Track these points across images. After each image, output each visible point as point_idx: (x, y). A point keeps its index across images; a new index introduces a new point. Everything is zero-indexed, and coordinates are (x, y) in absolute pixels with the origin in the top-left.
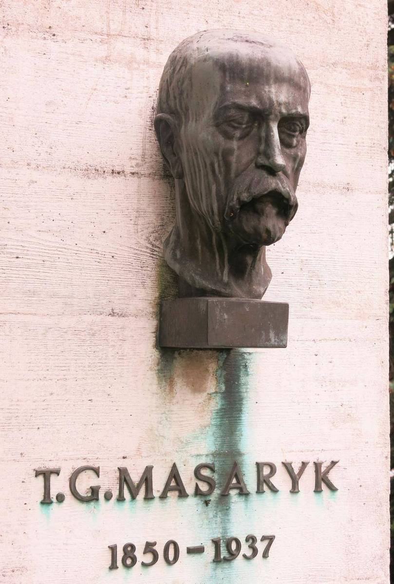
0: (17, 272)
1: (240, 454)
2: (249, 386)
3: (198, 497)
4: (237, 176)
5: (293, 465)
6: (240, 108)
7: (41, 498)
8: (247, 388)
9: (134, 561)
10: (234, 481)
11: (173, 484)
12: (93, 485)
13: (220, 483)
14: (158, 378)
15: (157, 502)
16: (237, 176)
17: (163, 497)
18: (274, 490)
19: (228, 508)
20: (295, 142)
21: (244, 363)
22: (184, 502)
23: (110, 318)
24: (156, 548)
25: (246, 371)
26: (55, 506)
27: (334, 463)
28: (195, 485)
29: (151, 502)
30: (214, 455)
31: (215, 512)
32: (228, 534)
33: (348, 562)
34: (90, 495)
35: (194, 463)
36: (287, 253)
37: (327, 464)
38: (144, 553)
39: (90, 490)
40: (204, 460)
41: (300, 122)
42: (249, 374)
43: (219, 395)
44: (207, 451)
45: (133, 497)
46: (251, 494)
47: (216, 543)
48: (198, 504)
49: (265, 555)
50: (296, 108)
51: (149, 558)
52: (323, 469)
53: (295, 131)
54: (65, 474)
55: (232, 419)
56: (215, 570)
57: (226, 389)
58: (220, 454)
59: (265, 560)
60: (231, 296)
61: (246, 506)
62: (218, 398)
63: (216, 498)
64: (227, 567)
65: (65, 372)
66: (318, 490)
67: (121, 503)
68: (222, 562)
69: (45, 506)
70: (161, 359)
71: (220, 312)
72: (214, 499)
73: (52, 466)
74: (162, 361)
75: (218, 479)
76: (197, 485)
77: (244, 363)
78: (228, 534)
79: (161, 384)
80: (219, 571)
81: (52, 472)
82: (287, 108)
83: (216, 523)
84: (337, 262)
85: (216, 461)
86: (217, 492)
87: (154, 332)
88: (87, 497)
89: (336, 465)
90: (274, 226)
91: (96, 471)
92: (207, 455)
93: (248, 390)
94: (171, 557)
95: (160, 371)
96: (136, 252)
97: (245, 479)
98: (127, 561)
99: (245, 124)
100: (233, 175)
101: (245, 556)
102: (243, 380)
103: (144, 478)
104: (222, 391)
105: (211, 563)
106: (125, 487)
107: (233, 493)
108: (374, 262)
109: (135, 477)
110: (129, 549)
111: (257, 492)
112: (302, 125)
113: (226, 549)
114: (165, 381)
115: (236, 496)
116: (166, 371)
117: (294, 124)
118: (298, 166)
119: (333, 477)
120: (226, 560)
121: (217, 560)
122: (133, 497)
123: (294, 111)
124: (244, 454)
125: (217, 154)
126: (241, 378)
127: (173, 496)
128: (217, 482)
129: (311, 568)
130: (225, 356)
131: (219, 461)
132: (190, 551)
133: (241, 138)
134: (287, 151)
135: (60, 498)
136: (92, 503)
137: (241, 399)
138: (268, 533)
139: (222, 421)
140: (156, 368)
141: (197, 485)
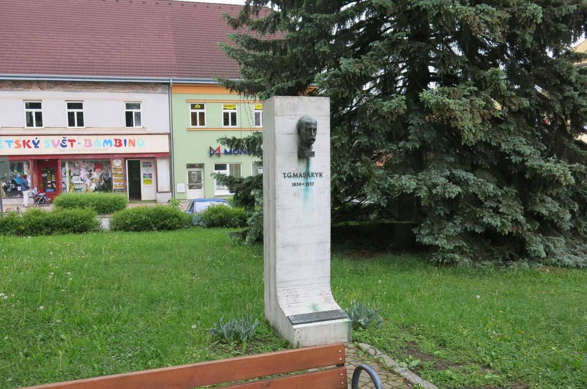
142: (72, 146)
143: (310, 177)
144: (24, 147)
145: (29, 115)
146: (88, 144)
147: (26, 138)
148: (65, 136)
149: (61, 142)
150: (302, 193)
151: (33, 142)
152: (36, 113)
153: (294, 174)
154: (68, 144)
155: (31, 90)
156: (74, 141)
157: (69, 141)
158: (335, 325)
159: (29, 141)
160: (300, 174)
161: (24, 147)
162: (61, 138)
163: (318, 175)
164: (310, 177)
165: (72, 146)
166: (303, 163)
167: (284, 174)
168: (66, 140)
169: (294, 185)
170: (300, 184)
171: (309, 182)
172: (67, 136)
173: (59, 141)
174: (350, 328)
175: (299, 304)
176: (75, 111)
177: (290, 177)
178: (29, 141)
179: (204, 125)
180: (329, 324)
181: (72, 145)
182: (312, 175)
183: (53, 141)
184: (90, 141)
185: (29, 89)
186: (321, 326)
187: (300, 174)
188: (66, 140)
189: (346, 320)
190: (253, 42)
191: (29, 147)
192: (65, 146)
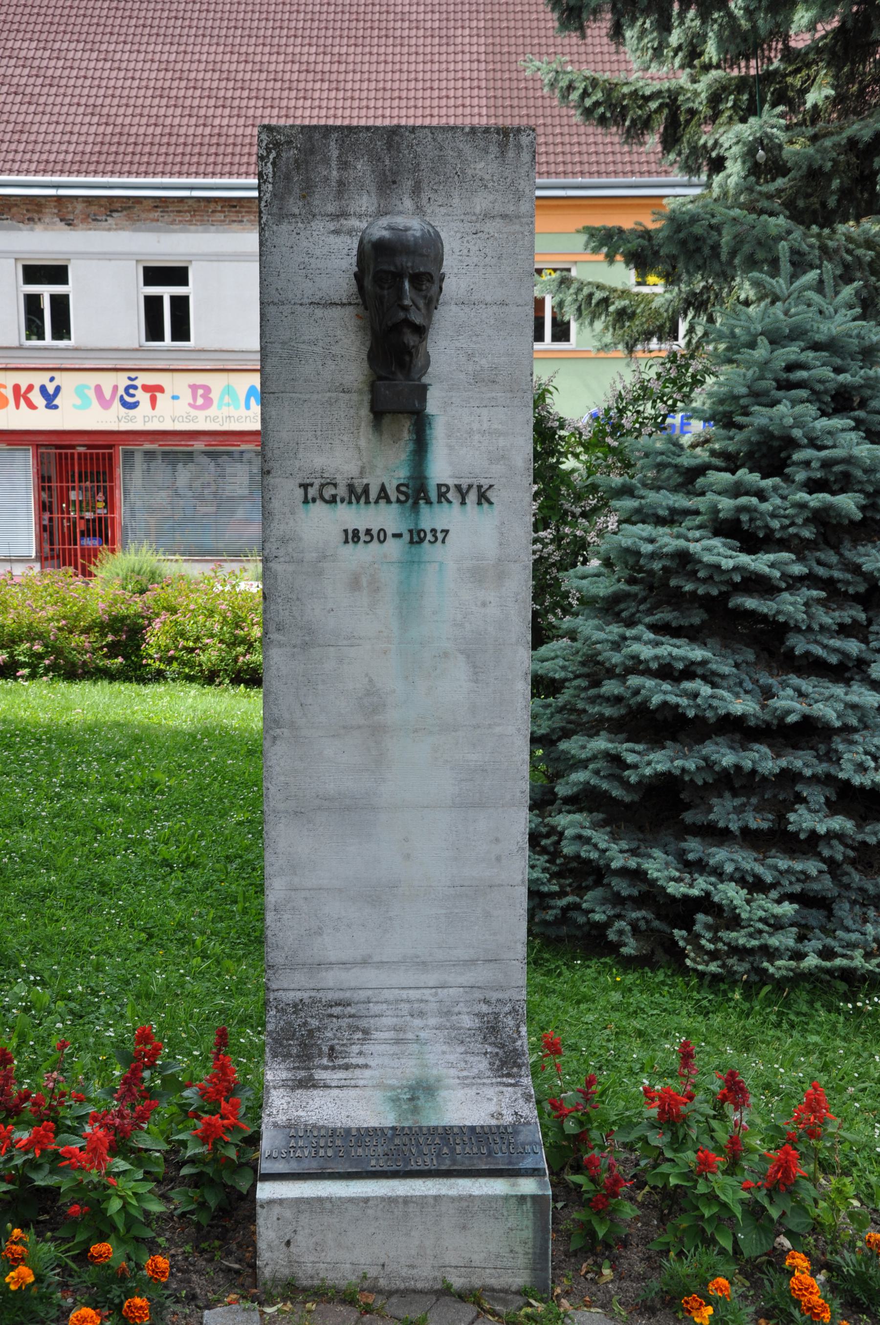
1: (425, 478)
17: (376, 502)
18: (449, 502)
27: (491, 486)
35: (395, 483)
45: (358, 502)
47: (411, 531)
49: (443, 541)
51: (368, 538)
54: (316, 486)
66: (479, 503)
86: (410, 501)
91: (335, 485)
94: (382, 538)
107: (422, 502)
109: (359, 490)
119: (489, 494)
121: (411, 542)
122: (358, 502)
135: (314, 500)
142: (153, 407)
143: (429, 502)
144: (17, 406)
145: (32, 303)
146: (200, 401)
147: (23, 380)
148: (133, 375)
149: (121, 391)
150: (390, 577)
151: (43, 389)
152: (54, 298)
153: (351, 488)
154: (142, 397)
155: (39, 227)
156: (160, 389)
157: (146, 388)
158: (467, 1201)
159: (30, 388)
160: (383, 488)
161: (17, 406)
162: (122, 380)
163: (472, 497)
164: (429, 502)
165: (153, 407)
166: (396, 439)
167: (305, 486)
168: (135, 387)
169: (353, 537)
170: (381, 536)
171: (439, 528)
172: (139, 374)
173: (116, 388)
174: (545, 1230)
175: (358, 1072)
176: (166, 292)
177: (333, 500)
178: (30, 388)
179: (568, 340)
180: (437, 1198)
181: (153, 401)
182: (442, 496)
183: (98, 389)
184: (207, 389)
185: (31, 224)
186: (391, 1201)
187: (383, 488)
188: (135, 387)
189: (528, 1186)
190: (696, 35)
191: (31, 406)
192: (134, 406)
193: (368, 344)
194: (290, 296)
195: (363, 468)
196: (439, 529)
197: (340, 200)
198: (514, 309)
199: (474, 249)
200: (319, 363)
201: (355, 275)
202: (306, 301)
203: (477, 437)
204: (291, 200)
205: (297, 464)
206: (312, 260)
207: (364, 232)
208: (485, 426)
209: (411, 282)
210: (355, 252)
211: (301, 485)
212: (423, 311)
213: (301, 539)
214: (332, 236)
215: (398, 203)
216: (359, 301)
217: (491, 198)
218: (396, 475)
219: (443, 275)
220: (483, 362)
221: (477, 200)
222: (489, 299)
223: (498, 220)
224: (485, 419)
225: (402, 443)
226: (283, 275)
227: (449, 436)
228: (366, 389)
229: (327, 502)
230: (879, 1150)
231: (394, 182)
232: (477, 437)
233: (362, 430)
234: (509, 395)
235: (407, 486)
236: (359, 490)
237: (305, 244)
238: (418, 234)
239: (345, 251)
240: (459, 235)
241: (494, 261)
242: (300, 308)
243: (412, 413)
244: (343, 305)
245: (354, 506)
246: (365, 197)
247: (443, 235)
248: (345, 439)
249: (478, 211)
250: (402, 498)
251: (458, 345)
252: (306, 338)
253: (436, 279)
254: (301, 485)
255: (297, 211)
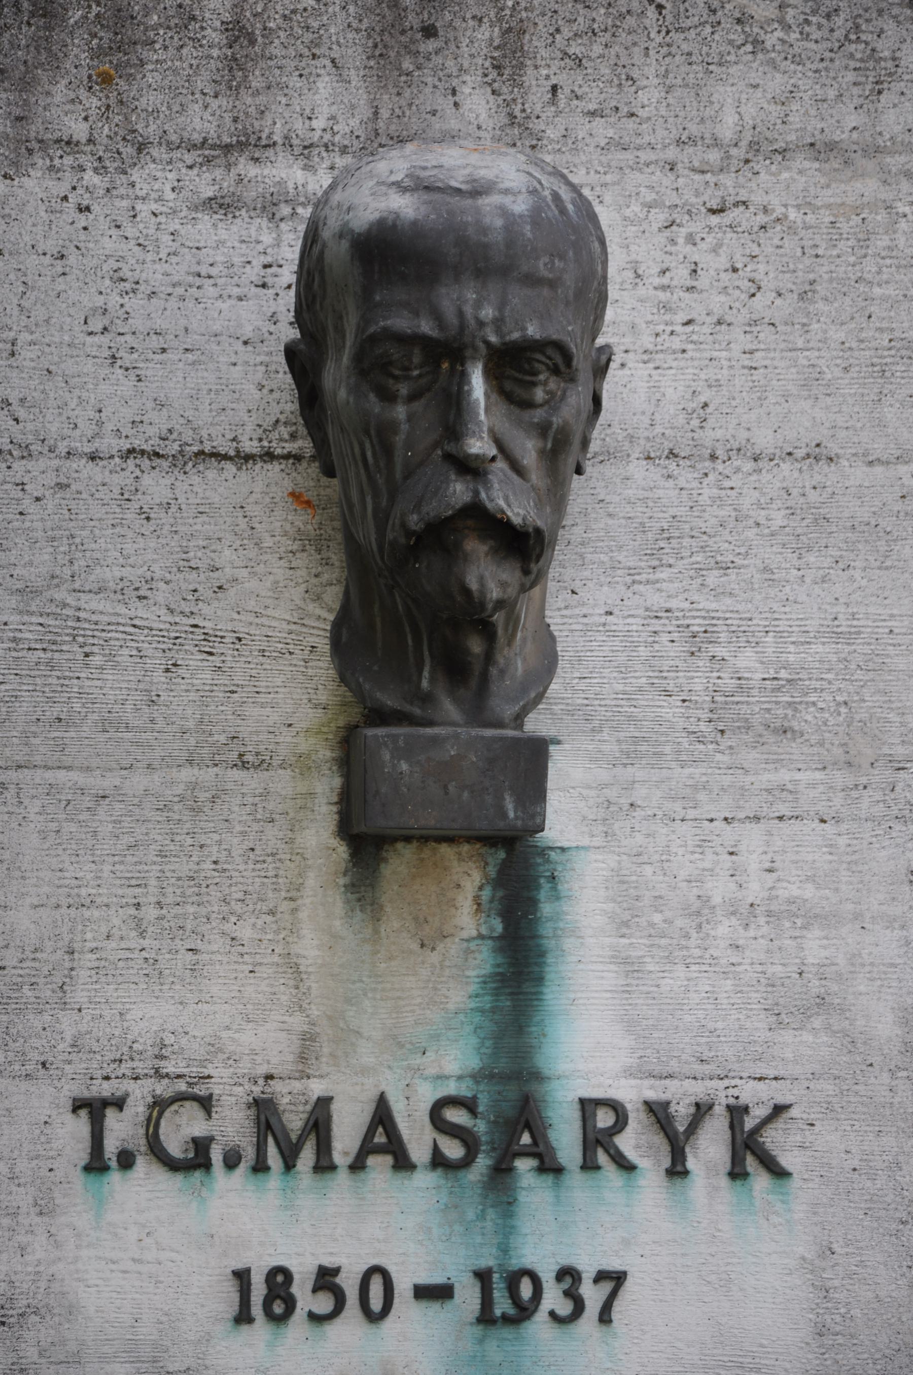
0: (30, 681)
1: (538, 1077)
2: (561, 925)
3: (439, 1171)
4: (406, 478)
5: (672, 1109)
6: (402, 339)
7: (83, 1157)
8: (555, 929)
9: (290, 1304)
10: (526, 1139)
11: (380, 1138)
12: (197, 1133)
13: (492, 1142)
14: (344, 903)
15: (342, 1176)
16: (406, 478)
17: (357, 1166)
18: (626, 1166)
19: (511, 1200)
20: (539, 394)
21: (548, 870)
22: (406, 1182)
23: (236, 774)
24: (339, 1280)
25: (554, 889)
26: (115, 1177)
27: (779, 1110)
28: (432, 1144)
29: (328, 1176)
30: (476, 1077)
31: (480, 1207)
32: (514, 1261)
33: (824, 1354)
34: (191, 1155)
35: (427, 1094)
36: (657, 617)
37: (759, 1113)
38: (315, 1290)
39: (191, 1145)
40: (452, 1089)
41: (544, 354)
42: (562, 895)
43: (490, 942)
44: (461, 1068)
45: (289, 1165)
46: (570, 1172)
47: (483, 1277)
48: (439, 1187)
49: (605, 1317)
50: (524, 329)
51: (324, 1304)
52: (749, 1123)
53: (535, 374)
54: (137, 1108)
55: (521, 997)
56: (481, 1341)
57: (505, 928)
58: (491, 1076)
59: (604, 1328)
60: (431, 723)
61: (557, 1197)
62: (484, 949)
63: (482, 1175)
64: (510, 1337)
65: (138, 891)
66: (737, 1173)
67: (260, 1176)
68: (499, 1324)
69: (92, 1177)
70: (351, 861)
71: (392, 757)
72: (479, 1178)
73: (106, 1089)
74: (354, 866)
75: (487, 1133)
76: (435, 1140)
77: (548, 870)
78: (514, 1261)
79: (352, 918)
80: (492, 1346)
81: (106, 1103)
82: (498, 331)
83: (483, 1234)
84: (785, 634)
85: (482, 1092)
86: (483, 1162)
87: (336, 803)
88: (186, 1159)
89: (785, 1115)
90: (481, 579)
91: (206, 1103)
92: (460, 1078)
93: (560, 932)
94: (376, 1304)
95: (352, 887)
96: (293, 627)
97: (552, 1135)
98: (283, 1306)
99: (416, 368)
100: (398, 475)
101: (552, 1314)
102: (546, 908)
103: (311, 1123)
104: (495, 934)
105: (471, 1324)
106: (270, 1140)
107: (524, 1165)
108: (887, 630)
109: (294, 1122)
110: (280, 1278)
111: (582, 1168)
112: (550, 358)
113: (507, 1294)
114: (361, 911)
115: (532, 1173)
116: (363, 888)
117: (530, 361)
118: (553, 445)
119: (772, 1138)
120: (507, 1320)
121: (486, 1318)
122: (289, 1165)
123: (516, 335)
124: (549, 1078)
125: (367, 432)
126: (542, 905)
127: (379, 1164)
128: (483, 1139)
129: (726, 1359)
130: (502, 855)
131: (489, 1092)
132: (423, 1293)
133: (412, 398)
134: (527, 415)
135: (126, 1160)
136: (198, 1175)
137: (542, 954)
138: (614, 1264)
139: (497, 1001)
140: (342, 881)
141: (435, 1140)
193: (333, 596)
194: (54, 427)
195: (308, 1039)
196: (588, 1268)
197: (235, 91)
198: (859, 474)
199: (713, 264)
200: (157, 661)
201: (291, 353)
202: (110, 444)
203: (724, 929)
204: (60, 92)
205: (68, 1025)
206: (133, 303)
207: (321, 203)
208: (755, 890)
209: (493, 375)
210: (288, 275)
211: (78, 1105)
212: (536, 477)
213: (71, 1310)
214: (205, 220)
215: (444, 104)
216: (304, 445)
217: (776, 83)
218: (430, 1063)
219: (607, 352)
220: (747, 660)
221: (724, 94)
222: (764, 440)
223: (801, 162)
224: (753, 862)
225: (453, 948)
226: (27, 354)
227: (623, 926)
228: (326, 753)
229: (173, 1165)
230: (911, 725)
231: (429, 32)
232: (724, 929)
233: (307, 901)
234: (840, 778)
235: (468, 1105)
236: (294, 1122)
237: (109, 245)
238: (520, 206)
239: (254, 273)
240: (659, 217)
241: (785, 307)
242: (89, 469)
243: (490, 841)
244: (244, 459)
245: (275, 1179)
246: (325, 85)
247: (605, 216)
248: (245, 932)
249: (727, 133)
250: (453, 1150)
251: (656, 600)
252: (110, 574)
253: (582, 364)
254: (78, 1105)
255: (79, 130)
